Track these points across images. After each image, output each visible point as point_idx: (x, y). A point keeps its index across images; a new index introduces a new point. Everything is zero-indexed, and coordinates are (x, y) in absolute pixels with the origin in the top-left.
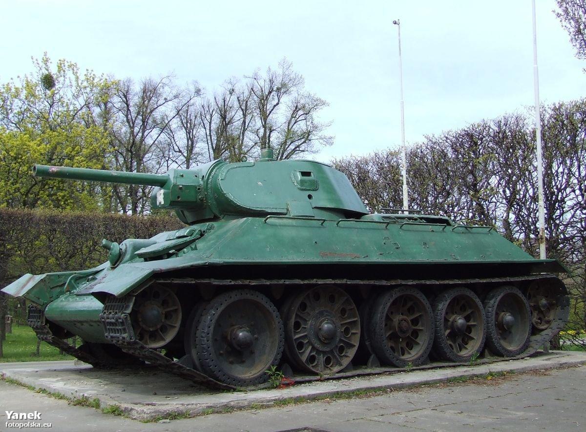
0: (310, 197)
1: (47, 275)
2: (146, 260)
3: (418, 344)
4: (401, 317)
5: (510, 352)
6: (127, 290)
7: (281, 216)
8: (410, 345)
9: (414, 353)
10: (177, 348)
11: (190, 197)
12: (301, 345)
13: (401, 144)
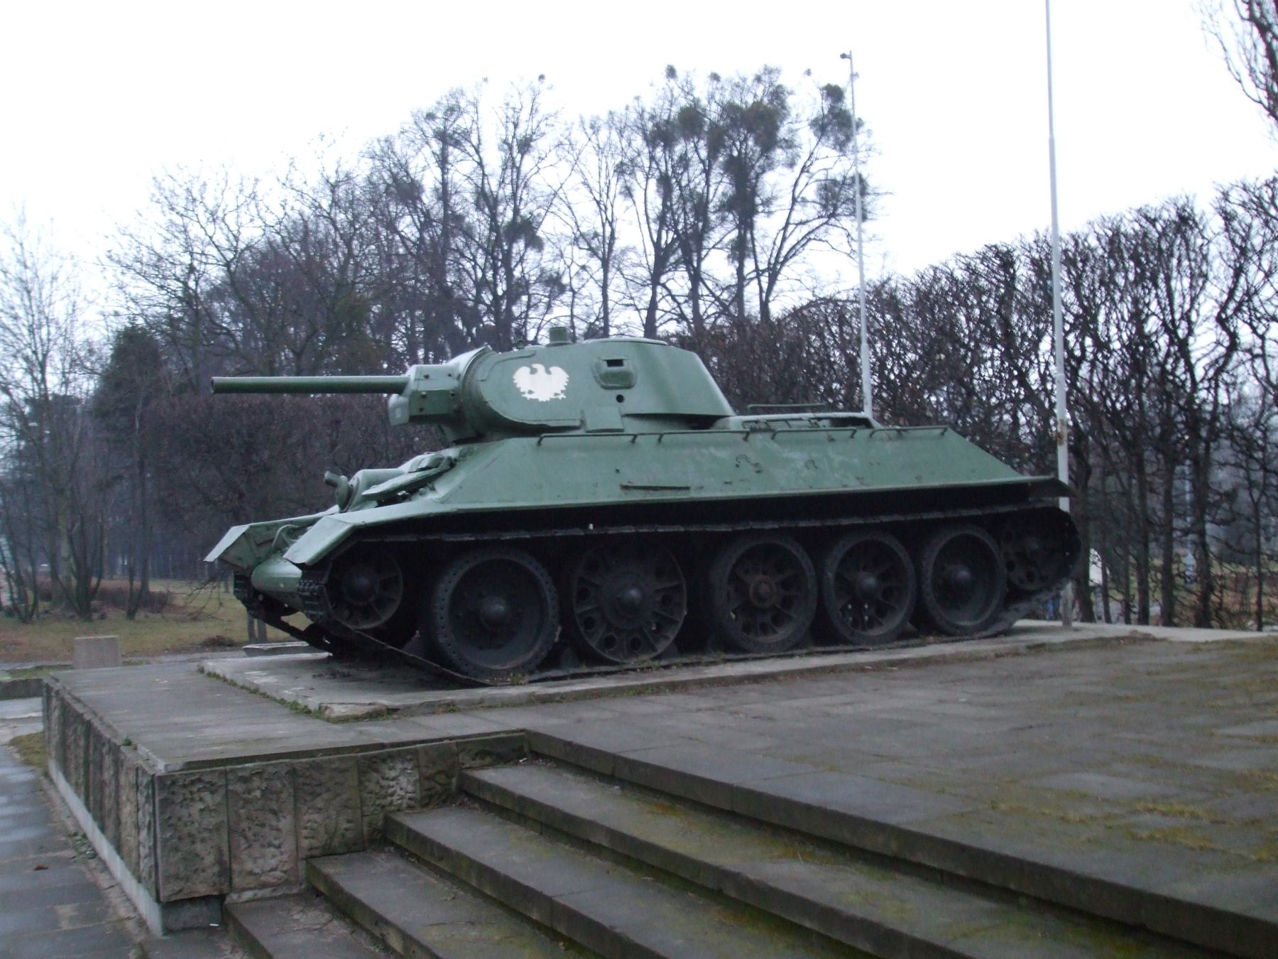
0: (620, 399)
1: (251, 527)
2: (381, 504)
3: (790, 618)
4: (760, 577)
5: (963, 628)
6: (319, 555)
7: (570, 433)
8: (779, 620)
9: (782, 633)
10: (397, 632)
11: (441, 408)
12: (589, 623)
13: (1043, 224)
